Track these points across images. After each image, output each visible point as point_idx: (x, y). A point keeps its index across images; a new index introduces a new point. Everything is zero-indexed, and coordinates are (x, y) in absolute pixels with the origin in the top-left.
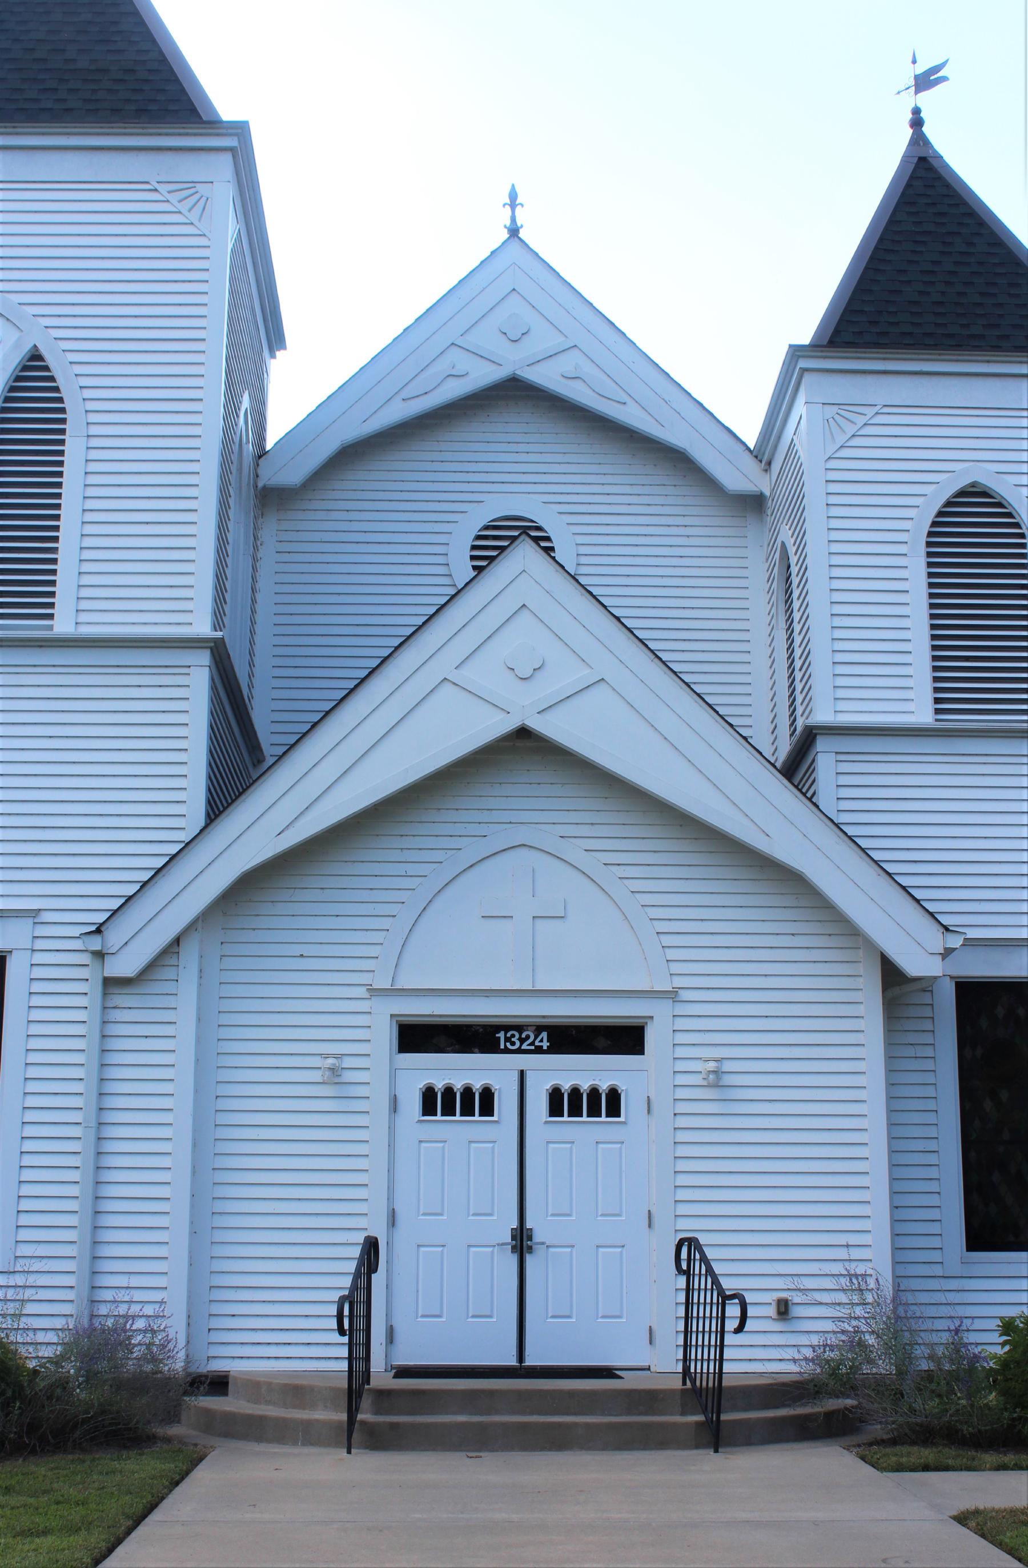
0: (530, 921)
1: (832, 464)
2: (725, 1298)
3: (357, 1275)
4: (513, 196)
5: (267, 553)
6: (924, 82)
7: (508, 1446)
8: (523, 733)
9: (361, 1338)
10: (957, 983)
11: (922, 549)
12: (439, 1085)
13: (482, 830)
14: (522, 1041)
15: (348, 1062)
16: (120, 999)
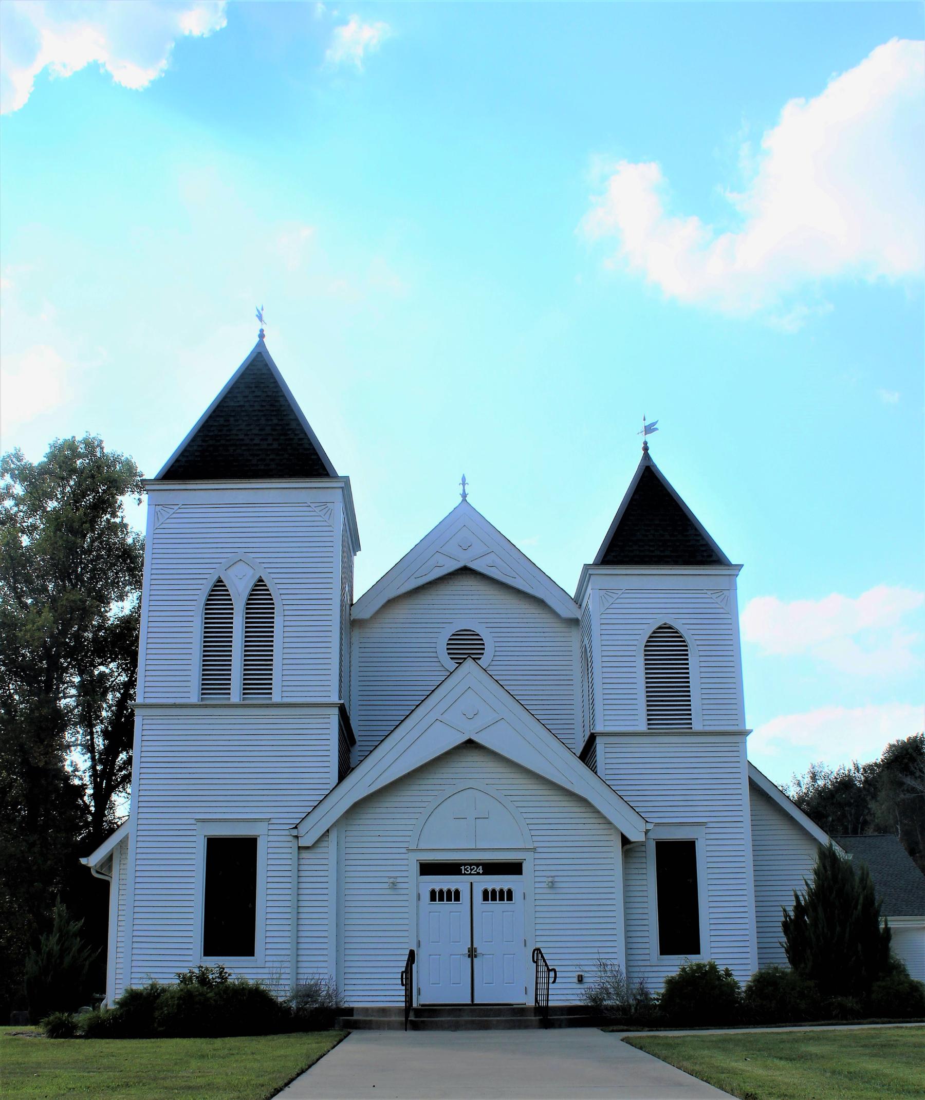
1: (603, 617)
2: (549, 970)
3: (407, 964)
4: (464, 479)
5: (355, 648)
6: (649, 429)
7: (467, 1029)
11: (643, 653)
13: (454, 782)
15: (399, 880)
16: (305, 854)
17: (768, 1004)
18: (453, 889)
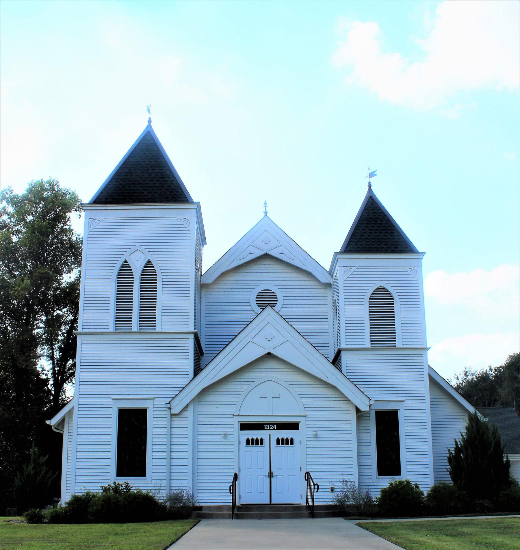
0: (269, 397)
1: (345, 282)
2: (314, 485)
4: (265, 203)
5: (203, 300)
6: (371, 175)
8: (269, 354)
9: (234, 494)
10: (376, 412)
11: (368, 303)
12: (280, 438)
13: (260, 377)
14: (270, 427)
15: (228, 433)
16: (174, 418)
17: (441, 504)
18: (259, 438)
